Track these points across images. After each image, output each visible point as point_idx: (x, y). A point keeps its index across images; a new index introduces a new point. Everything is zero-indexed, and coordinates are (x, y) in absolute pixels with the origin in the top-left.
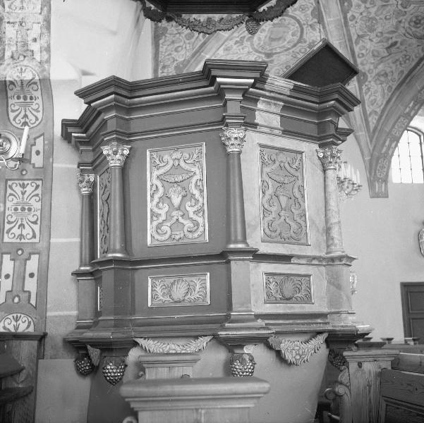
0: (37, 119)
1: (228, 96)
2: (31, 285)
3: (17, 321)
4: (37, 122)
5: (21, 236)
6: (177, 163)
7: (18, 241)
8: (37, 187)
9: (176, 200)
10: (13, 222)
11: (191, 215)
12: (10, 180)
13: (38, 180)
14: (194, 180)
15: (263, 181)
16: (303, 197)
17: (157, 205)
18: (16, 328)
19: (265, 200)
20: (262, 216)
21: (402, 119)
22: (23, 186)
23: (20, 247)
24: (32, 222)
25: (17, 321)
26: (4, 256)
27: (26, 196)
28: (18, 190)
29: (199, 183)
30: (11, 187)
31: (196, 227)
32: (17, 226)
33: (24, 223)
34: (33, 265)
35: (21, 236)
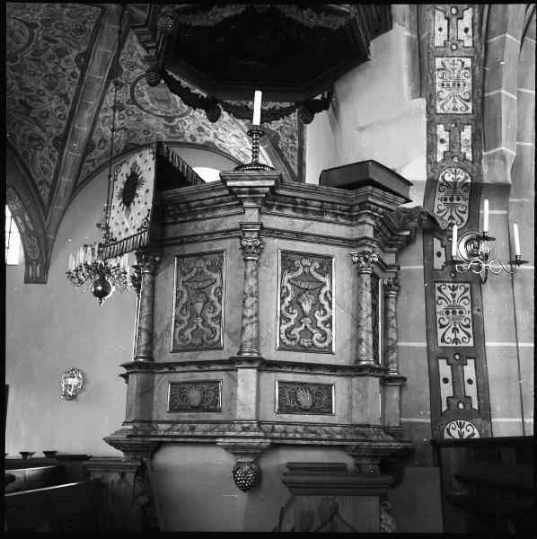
0: (462, 221)
1: (246, 204)
2: (471, 391)
3: (461, 428)
4: (463, 224)
5: (456, 340)
6: (200, 270)
7: (454, 345)
8: (466, 290)
9: (307, 307)
10: (445, 326)
11: (319, 324)
12: (438, 282)
13: (467, 282)
14: (324, 291)
15: (282, 288)
16: (330, 304)
17: (287, 308)
18: (461, 435)
19: (283, 307)
20: (278, 323)
21: (118, 240)
22: (454, 289)
23: (457, 351)
24: (465, 326)
25: (461, 428)
26: (440, 361)
27: (456, 299)
28: (448, 292)
29: (329, 295)
30: (439, 289)
31: (324, 338)
32: (450, 330)
33: (458, 326)
34: (469, 370)
35: (456, 340)
